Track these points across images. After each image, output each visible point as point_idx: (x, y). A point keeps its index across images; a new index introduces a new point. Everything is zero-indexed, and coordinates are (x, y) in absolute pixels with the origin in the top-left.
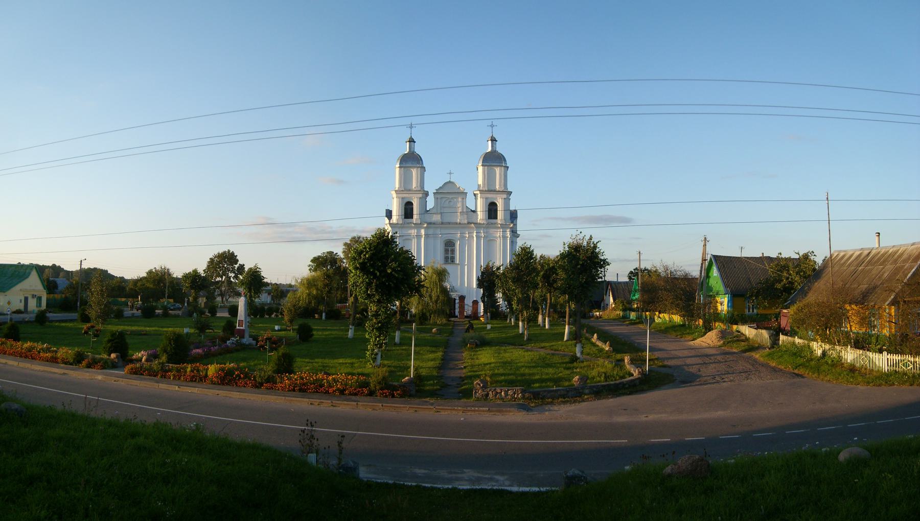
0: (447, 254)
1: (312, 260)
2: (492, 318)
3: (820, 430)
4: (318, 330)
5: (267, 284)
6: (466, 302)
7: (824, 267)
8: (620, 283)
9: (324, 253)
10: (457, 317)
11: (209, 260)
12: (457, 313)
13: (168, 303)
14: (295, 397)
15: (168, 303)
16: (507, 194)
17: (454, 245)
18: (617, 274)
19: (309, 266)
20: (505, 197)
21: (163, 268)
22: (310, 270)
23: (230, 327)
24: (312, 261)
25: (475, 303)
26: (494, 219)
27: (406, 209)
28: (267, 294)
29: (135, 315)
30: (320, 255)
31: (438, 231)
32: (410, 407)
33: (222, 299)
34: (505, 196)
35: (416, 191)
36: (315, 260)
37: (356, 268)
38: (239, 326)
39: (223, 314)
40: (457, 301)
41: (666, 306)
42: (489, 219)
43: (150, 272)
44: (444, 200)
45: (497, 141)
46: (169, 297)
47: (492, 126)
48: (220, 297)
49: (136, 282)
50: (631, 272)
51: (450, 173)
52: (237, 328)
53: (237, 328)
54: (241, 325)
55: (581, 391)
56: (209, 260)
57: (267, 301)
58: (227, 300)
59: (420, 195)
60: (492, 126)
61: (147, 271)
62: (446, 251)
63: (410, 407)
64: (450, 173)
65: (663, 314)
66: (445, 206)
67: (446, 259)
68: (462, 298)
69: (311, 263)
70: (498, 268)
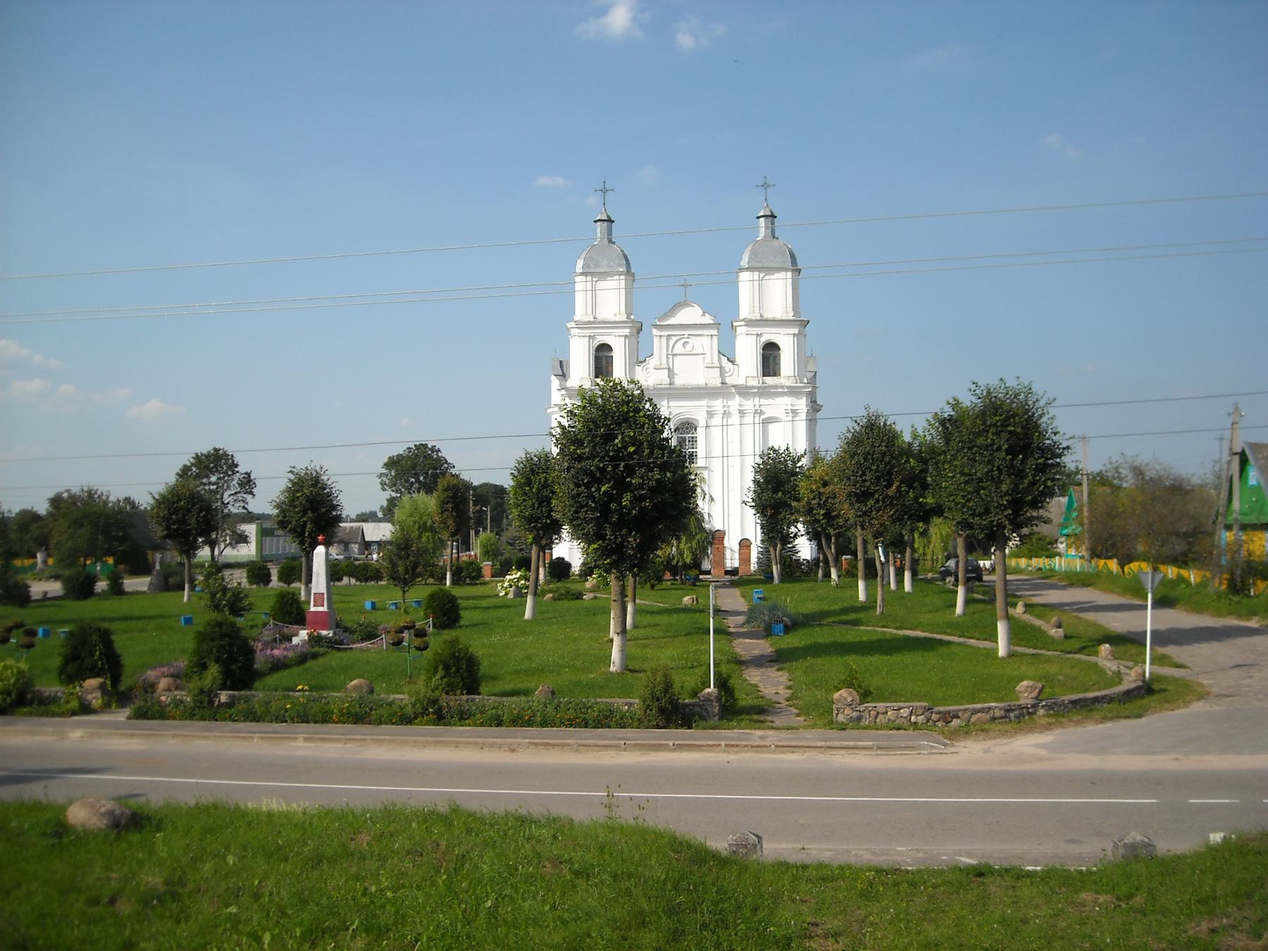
1: (385, 465)
4: (1060, 561)
7: (761, 711)
14: (501, 738)
16: (800, 325)
18: (561, 362)
20: (797, 332)
22: (383, 484)
24: (386, 465)
26: (775, 375)
29: (48, 596)
30: (402, 452)
32: (726, 745)
33: (213, 551)
36: (392, 463)
38: (315, 606)
44: (675, 339)
53: (313, 609)
59: (627, 331)
63: (726, 745)
66: (674, 352)
69: (384, 471)
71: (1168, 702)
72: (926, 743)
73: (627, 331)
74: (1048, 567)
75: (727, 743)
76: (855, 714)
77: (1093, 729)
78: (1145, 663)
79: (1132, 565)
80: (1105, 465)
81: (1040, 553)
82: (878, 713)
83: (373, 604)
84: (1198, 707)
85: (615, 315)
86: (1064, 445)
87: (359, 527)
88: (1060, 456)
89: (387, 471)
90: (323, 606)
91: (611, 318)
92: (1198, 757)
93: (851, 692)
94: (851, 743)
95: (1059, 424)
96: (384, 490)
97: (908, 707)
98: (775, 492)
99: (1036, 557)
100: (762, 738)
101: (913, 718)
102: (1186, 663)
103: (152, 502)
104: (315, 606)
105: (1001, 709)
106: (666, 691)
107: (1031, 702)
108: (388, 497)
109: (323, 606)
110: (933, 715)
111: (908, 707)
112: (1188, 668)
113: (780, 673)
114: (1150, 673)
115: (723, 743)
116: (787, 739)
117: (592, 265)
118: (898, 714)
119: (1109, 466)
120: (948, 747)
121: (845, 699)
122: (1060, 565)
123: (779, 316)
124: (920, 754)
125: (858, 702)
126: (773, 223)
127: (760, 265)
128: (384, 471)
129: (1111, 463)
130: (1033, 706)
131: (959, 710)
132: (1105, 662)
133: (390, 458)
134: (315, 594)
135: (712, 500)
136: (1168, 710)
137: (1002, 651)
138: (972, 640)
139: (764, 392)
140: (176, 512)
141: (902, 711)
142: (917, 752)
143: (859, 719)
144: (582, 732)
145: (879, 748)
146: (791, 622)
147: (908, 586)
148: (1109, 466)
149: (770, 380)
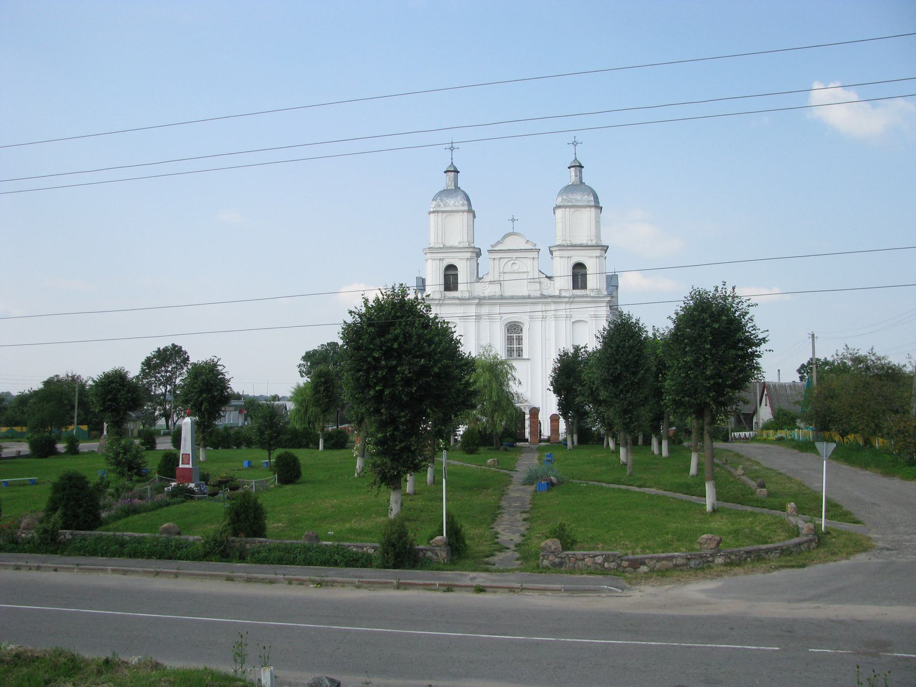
0: (511, 345)
2: (580, 442)
3: (812, 652)
5: (238, 397)
6: (541, 417)
8: (782, 386)
9: (323, 345)
10: (527, 440)
11: (146, 358)
12: (527, 435)
13: (79, 430)
15: (79, 430)
17: (521, 330)
19: (299, 366)
21: (70, 375)
23: (170, 462)
24: (304, 358)
25: (554, 419)
26: (582, 288)
27: (446, 276)
28: (237, 412)
29: (21, 454)
31: (497, 309)
34: (598, 253)
35: (461, 248)
36: (308, 356)
37: (352, 379)
38: (182, 464)
39: (164, 444)
40: (527, 416)
41: (402, 544)
42: (573, 289)
43: (48, 383)
45: (583, 167)
46: (81, 423)
47: (575, 144)
48: (164, 419)
49: (23, 400)
50: (803, 366)
51: (513, 220)
52: (181, 466)
54: (186, 461)
55: (710, 559)
56: (146, 358)
57: (238, 424)
58: (175, 424)
59: (468, 255)
60: (575, 144)
61: (45, 379)
62: (510, 340)
64: (513, 220)
65: (853, 435)
66: (505, 271)
67: (510, 351)
68: (535, 412)
69: (302, 362)
70: (456, 416)
71: (833, 554)
72: (606, 587)
73: (468, 255)
74: (790, 437)
75: (441, 582)
76: (557, 560)
77: (758, 577)
78: (822, 518)
79: (849, 436)
80: (833, 356)
81: (784, 427)
82: (577, 559)
83: (249, 463)
84: (862, 558)
85: (460, 243)
86: (760, 337)
87: (284, 404)
88: (758, 345)
89: (304, 363)
90: (189, 464)
91: (456, 244)
92: (837, 606)
93: (555, 542)
94: (543, 586)
95: (757, 322)
96: (302, 376)
97: (602, 555)
98: (568, 378)
99: (781, 429)
100: (472, 579)
101: (606, 564)
102: (861, 519)
103: (84, 381)
104: (182, 464)
105: (682, 558)
106: (400, 538)
107: (710, 552)
108: (305, 381)
109: (189, 464)
110: (623, 562)
111: (602, 555)
112: (863, 524)
113: (524, 523)
114: (825, 527)
115: (437, 583)
116: (494, 581)
117: (442, 205)
118: (594, 560)
119: (836, 357)
120: (625, 591)
121: (550, 547)
122: (798, 435)
123: (584, 242)
124: (599, 596)
125: (561, 549)
126: (581, 172)
127: (570, 204)
128: (302, 362)
129: (837, 354)
130: (711, 555)
131: (646, 558)
132: (791, 519)
133: (307, 353)
134: (183, 454)
135: (520, 383)
136: (831, 561)
137: (709, 508)
138: (694, 497)
139: (572, 300)
140: (110, 392)
141: (596, 558)
142: (596, 594)
143: (561, 564)
144: (326, 569)
145: (566, 590)
146: (557, 479)
147: (665, 453)
148: (836, 357)
149: (578, 292)
